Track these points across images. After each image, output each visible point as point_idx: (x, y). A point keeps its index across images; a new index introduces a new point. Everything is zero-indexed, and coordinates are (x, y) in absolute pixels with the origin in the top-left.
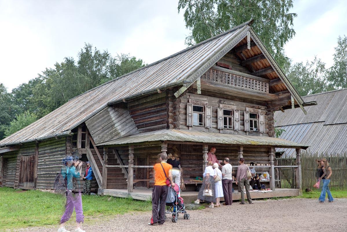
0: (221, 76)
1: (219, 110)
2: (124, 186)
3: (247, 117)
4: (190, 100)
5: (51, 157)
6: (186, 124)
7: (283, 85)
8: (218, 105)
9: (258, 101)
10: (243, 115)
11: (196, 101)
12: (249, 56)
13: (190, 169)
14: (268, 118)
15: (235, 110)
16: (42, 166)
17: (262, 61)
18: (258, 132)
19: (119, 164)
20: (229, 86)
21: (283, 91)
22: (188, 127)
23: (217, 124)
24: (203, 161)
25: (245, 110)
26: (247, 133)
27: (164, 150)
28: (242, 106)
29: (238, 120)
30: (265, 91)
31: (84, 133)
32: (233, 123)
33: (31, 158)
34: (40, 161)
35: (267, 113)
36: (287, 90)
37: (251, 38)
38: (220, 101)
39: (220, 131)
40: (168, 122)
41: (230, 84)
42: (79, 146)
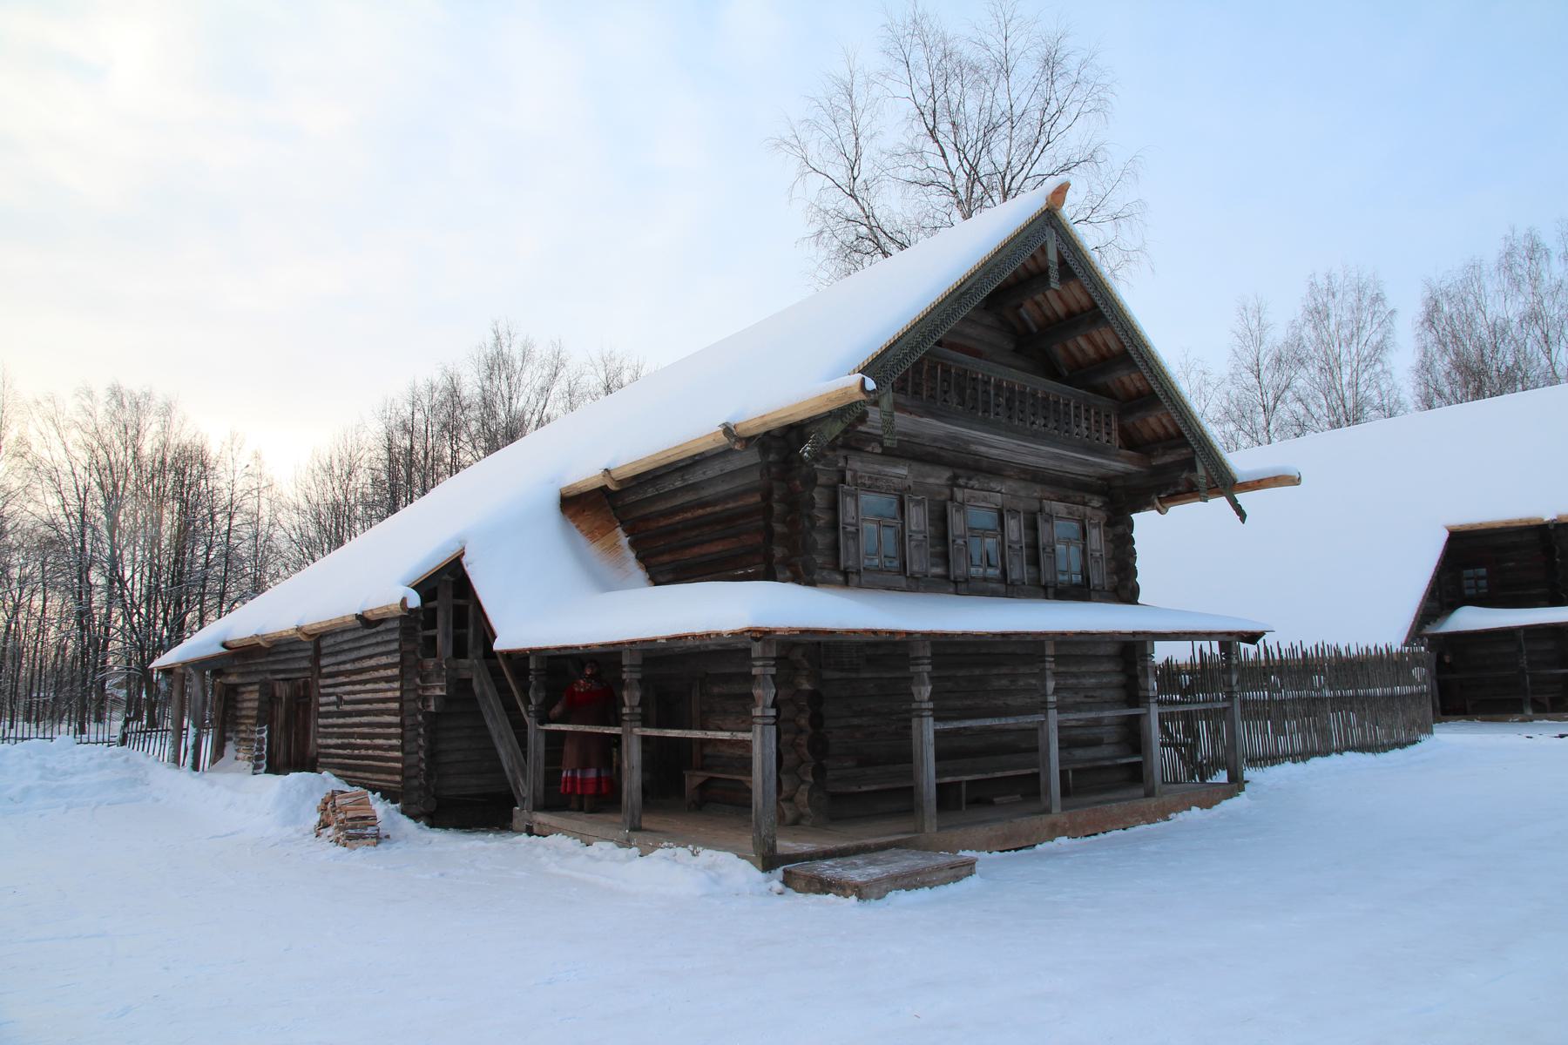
6: (838, 564)
7: (1165, 421)
9: (1080, 477)
15: (1008, 511)
17: (1095, 334)
25: (1041, 511)
26: (1050, 591)
28: (1028, 495)
30: (1108, 442)
33: (299, 687)
36: (1181, 434)
37: (1059, 253)
38: (955, 477)
39: (959, 587)
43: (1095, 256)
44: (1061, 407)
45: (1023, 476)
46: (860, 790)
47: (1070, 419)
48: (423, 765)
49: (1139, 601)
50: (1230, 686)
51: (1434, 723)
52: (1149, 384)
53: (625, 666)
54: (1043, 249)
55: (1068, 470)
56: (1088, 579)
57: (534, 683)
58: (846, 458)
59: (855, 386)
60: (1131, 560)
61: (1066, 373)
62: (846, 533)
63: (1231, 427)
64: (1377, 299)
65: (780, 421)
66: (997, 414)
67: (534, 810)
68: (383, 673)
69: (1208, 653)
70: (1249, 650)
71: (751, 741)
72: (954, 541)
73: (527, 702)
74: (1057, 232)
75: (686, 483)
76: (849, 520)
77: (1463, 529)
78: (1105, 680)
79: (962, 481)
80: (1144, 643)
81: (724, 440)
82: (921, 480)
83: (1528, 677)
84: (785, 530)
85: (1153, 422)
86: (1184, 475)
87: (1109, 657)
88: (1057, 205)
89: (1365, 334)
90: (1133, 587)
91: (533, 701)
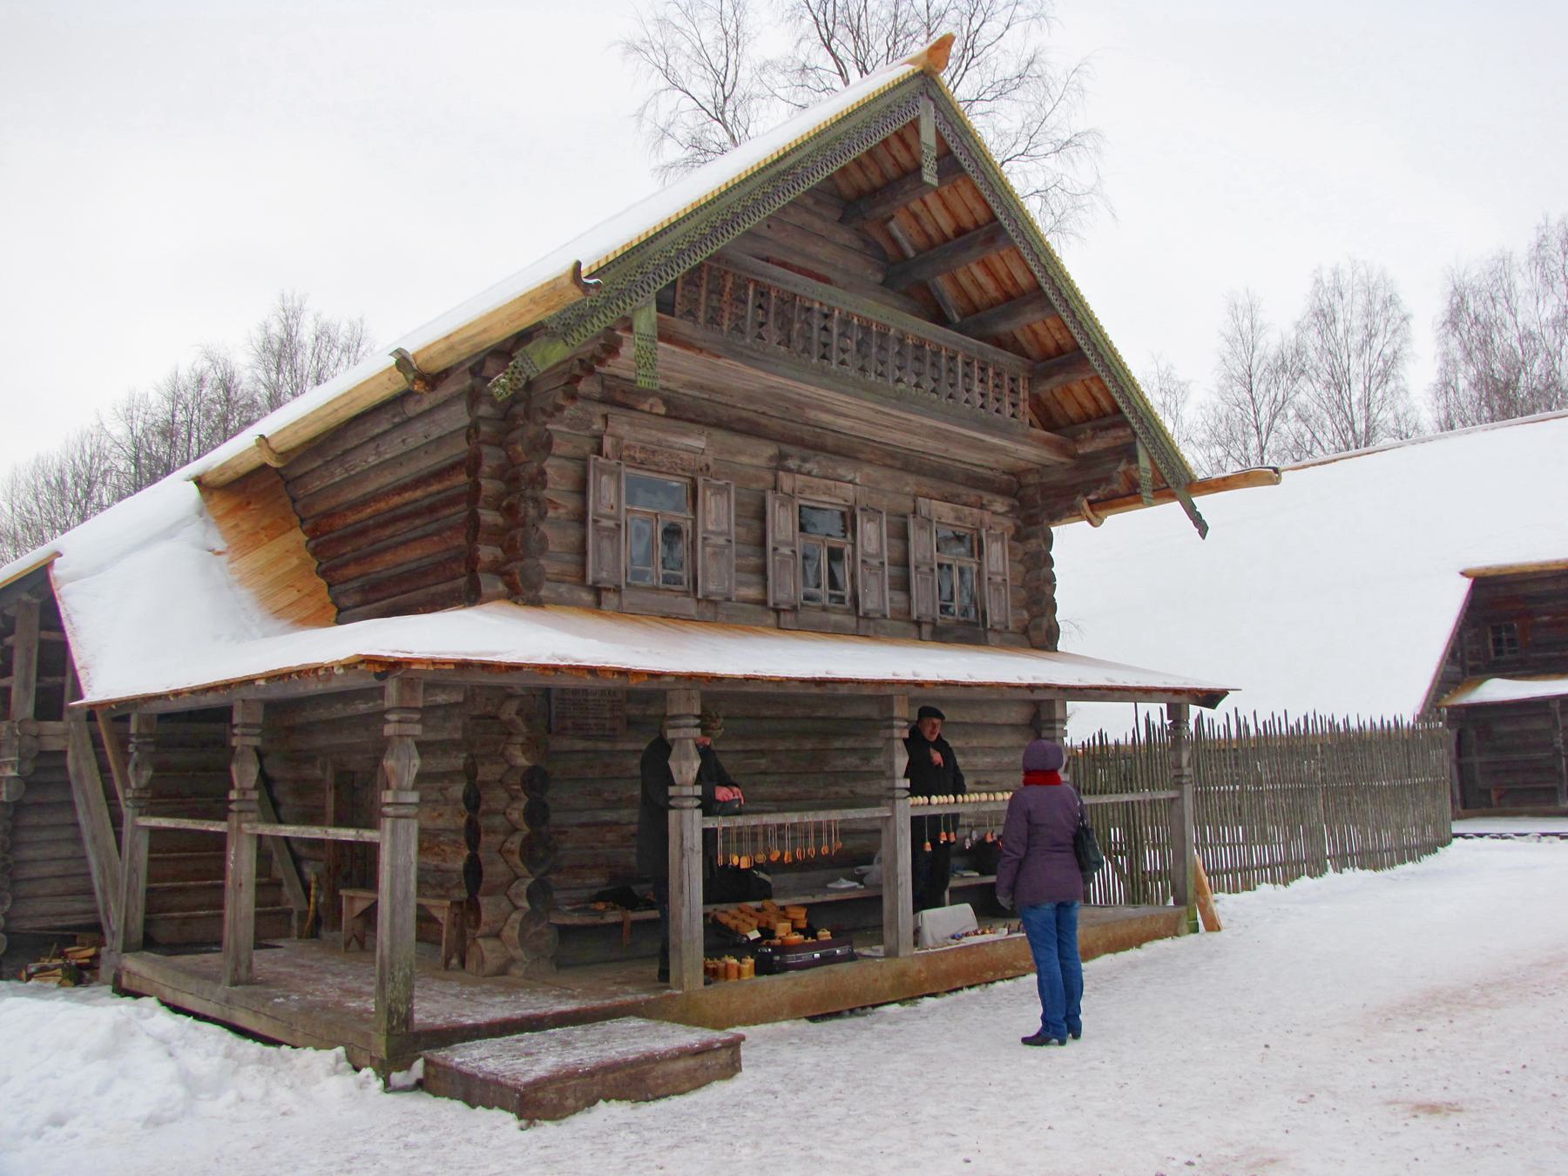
6: (584, 576)
9: (975, 469)
10: (904, 537)
11: (643, 448)
12: (929, 237)
13: (610, 837)
14: (1026, 554)
21: (1099, 418)
22: (597, 590)
23: (766, 579)
24: (672, 791)
25: (915, 512)
26: (926, 629)
28: (896, 490)
35: (1018, 530)
36: (1118, 410)
37: (938, 132)
38: (782, 457)
41: (834, 362)
43: (1033, 206)
44: (943, 360)
45: (889, 461)
46: (602, 922)
47: (956, 378)
49: (1060, 646)
50: (1180, 767)
51: (1453, 819)
52: (1072, 337)
53: (236, 726)
54: (914, 125)
55: (958, 458)
56: (984, 614)
57: (136, 754)
59: (565, 275)
60: (1047, 589)
61: (957, 319)
62: (598, 530)
63: (1218, 451)
64: (1390, 302)
65: (472, 342)
66: (843, 363)
67: (123, 952)
68: (1100, 823)
69: (1158, 724)
70: (1217, 718)
71: (379, 844)
72: (775, 549)
74: (936, 107)
75: (381, 459)
76: (605, 510)
77: (1490, 573)
78: (1006, 760)
80: (1051, 702)
81: (400, 383)
82: (727, 457)
83: (1564, 759)
84: (500, 520)
85: (1027, 323)
86: (1122, 467)
87: (1014, 727)
88: (936, 66)
89: (1377, 343)
90: (1050, 626)
91: (133, 785)
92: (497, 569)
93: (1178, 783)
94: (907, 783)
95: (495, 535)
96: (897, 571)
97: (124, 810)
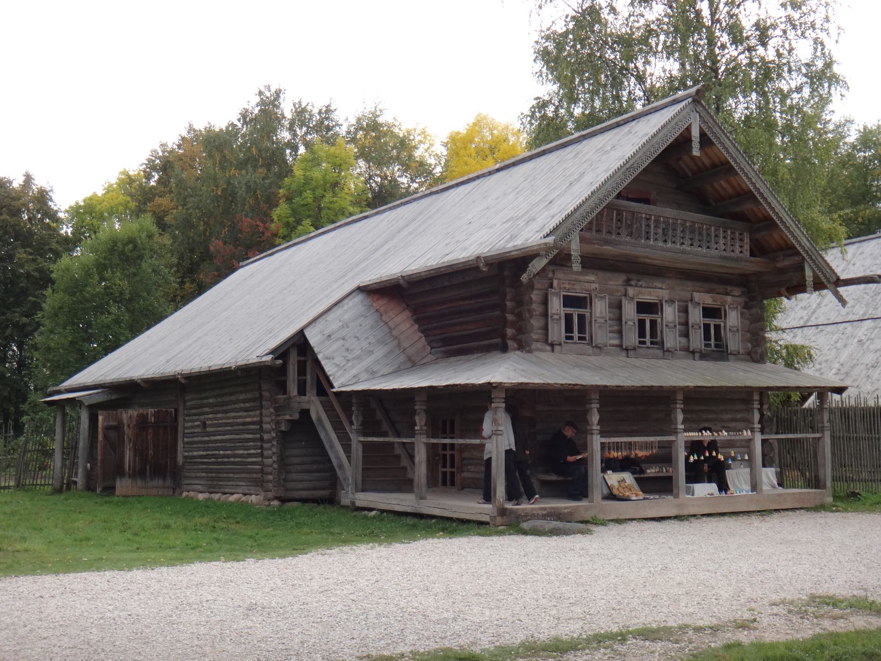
0: (629, 222)
1: (627, 302)
2: (404, 485)
3: (696, 316)
4: (555, 283)
5: (219, 415)
6: (547, 339)
8: (624, 291)
9: (724, 275)
15: (666, 301)
16: (195, 437)
17: (732, 179)
18: (723, 352)
19: (385, 435)
20: (648, 247)
24: (589, 428)
25: (692, 300)
26: (697, 355)
27: (497, 405)
28: (683, 290)
29: (672, 325)
30: (741, 252)
31: (302, 358)
32: (662, 332)
34: (190, 424)
35: (746, 303)
37: (701, 128)
40: (504, 337)
42: (293, 389)
48: (276, 466)
50: (823, 422)
58: (553, 272)
62: (552, 320)
72: (626, 323)
73: (351, 423)
79: (633, 283)
92: (513, 338)
93: (823, 431)
94: (682, 427)
95: (513, 324)
96: (682, 328)
97: (351, 436)
